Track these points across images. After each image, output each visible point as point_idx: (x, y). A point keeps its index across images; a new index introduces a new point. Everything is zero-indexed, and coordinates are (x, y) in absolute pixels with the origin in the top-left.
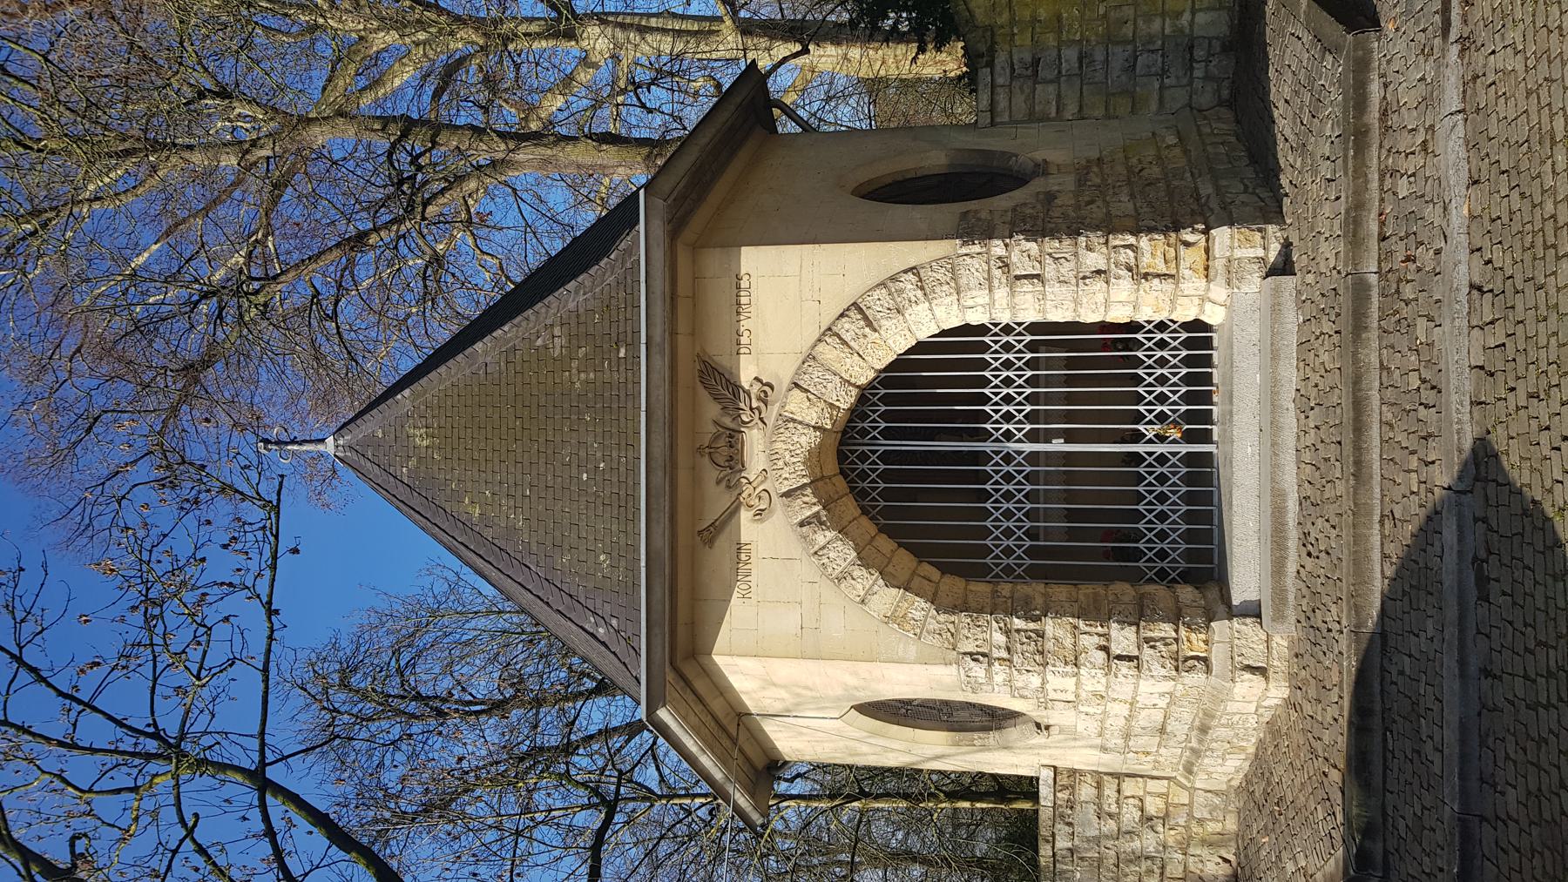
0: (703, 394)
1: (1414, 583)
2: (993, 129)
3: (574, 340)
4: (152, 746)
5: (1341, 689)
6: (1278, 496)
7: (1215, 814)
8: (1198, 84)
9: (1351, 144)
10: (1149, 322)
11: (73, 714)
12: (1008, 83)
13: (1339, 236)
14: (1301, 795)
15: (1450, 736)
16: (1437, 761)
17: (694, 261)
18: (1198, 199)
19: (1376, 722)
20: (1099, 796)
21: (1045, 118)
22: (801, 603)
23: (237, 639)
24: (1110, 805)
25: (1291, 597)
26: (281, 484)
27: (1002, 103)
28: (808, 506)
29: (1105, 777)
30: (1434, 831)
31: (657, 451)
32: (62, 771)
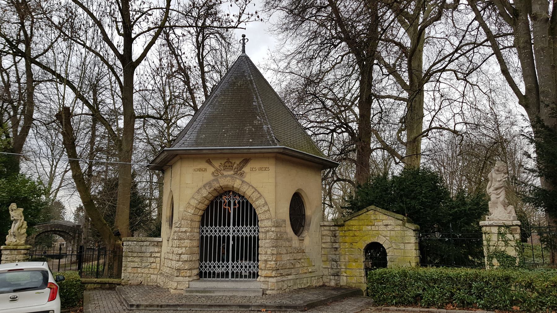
6: (213, 292)
8: (329, 277)
19: (159, 308)
25: (191, 294)
27: (325, 228)
28: (216, 185)
31: (225, 151)
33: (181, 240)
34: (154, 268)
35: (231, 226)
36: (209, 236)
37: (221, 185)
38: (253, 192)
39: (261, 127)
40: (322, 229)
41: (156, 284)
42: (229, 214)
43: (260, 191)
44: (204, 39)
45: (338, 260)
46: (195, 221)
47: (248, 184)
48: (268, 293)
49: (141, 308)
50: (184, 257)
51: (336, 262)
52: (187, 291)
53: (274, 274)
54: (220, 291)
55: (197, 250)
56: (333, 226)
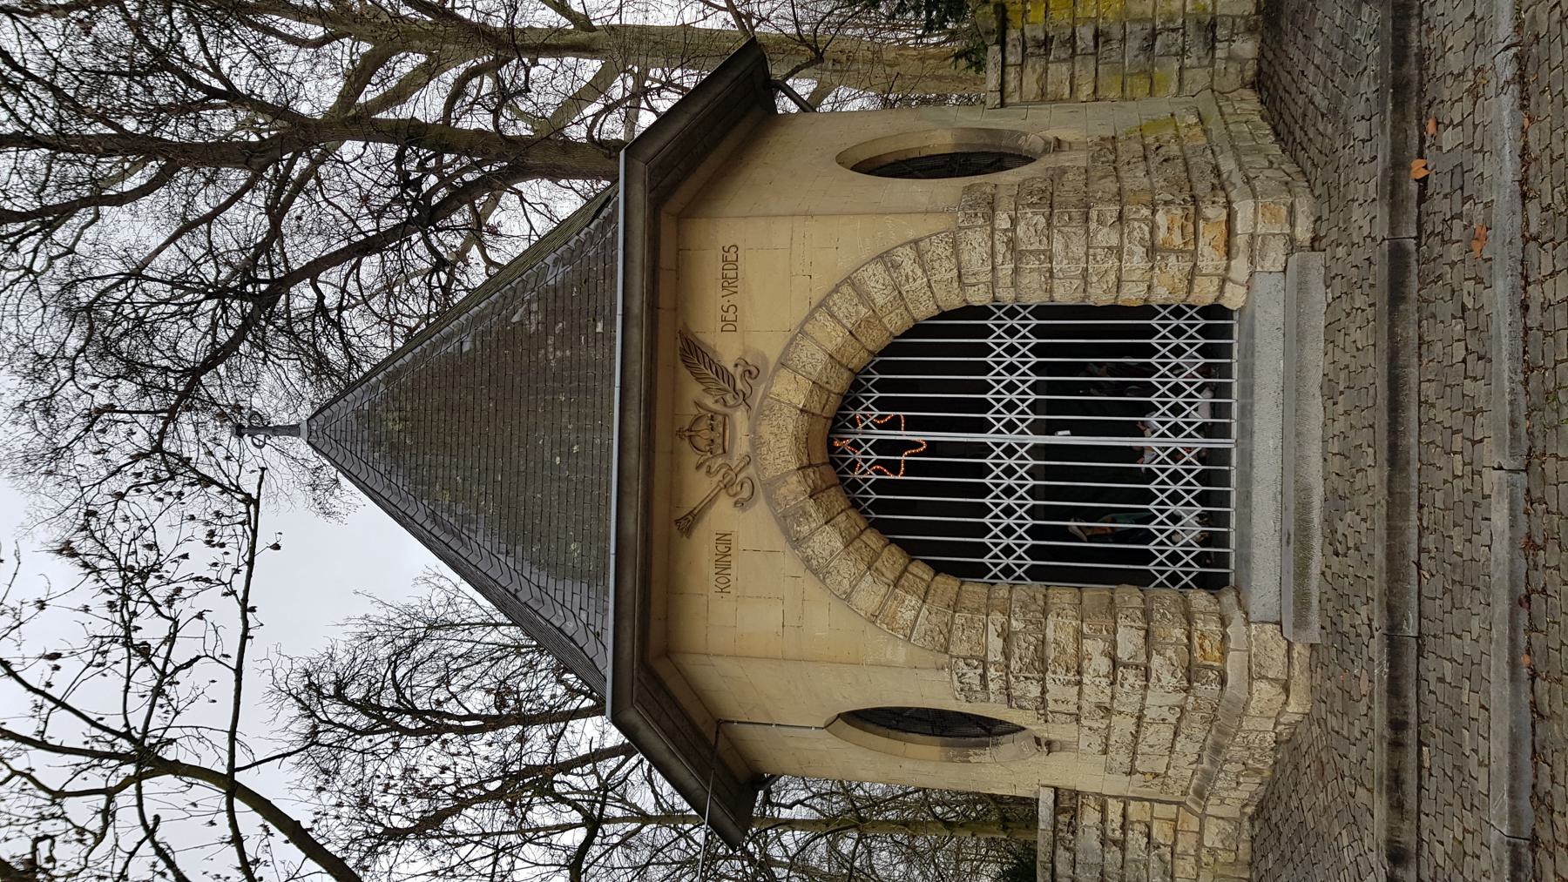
0: (685, 373)
1: (1457, 578)
2: (1003, 110)
3: (550, 316)
4: (124, 746)
5: (1372, 699)
6: (1304, 491)
7: (1227, 843)
8: (1220, 65)
9: (1390, 97)
10: (1164, 307)
11: (45, 711)
12: (1020, 61)
13: (1374, 200)
14: (1323, 820)
15: (1498, 748)
16: (1483, 777)
17: (678, 231)
18: (1219, 175)
19: (1411, 736)
20: (1103, 821)
21: (1058, 100)
22: (783, 600)
23: (211, 635)
24: (1113, 830)
25: (1315, 602)
26: (262, 478)
27: (1012, 84)
28: (794, 488)
29: (1110, 801)
30: (1478, 857)
32: (32, 770)
33: (1043, 661)
34: (1175, 831)
35: (988, 438)
36: (1030, 542)
37: (793, 467)
38: (832, 316)
39: (551, 294)
40: (1016, 99)
41: (1246, 824)
42: (933, 448)
43: (827, 287)
44: (415, 713)
45: (1149, 26)
46: (958, 594)
47: (793, 339)
48: (1309, 235)
49: (1408, 839)
50: (1129, 641)
51: (1154, 34)
52: (1301, 622)
53: (1215, 213)
54: (1301, 459)
55: (1094, 593)
56: (1003, 51)
